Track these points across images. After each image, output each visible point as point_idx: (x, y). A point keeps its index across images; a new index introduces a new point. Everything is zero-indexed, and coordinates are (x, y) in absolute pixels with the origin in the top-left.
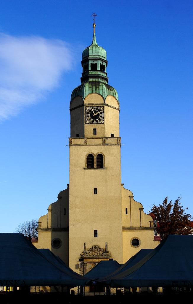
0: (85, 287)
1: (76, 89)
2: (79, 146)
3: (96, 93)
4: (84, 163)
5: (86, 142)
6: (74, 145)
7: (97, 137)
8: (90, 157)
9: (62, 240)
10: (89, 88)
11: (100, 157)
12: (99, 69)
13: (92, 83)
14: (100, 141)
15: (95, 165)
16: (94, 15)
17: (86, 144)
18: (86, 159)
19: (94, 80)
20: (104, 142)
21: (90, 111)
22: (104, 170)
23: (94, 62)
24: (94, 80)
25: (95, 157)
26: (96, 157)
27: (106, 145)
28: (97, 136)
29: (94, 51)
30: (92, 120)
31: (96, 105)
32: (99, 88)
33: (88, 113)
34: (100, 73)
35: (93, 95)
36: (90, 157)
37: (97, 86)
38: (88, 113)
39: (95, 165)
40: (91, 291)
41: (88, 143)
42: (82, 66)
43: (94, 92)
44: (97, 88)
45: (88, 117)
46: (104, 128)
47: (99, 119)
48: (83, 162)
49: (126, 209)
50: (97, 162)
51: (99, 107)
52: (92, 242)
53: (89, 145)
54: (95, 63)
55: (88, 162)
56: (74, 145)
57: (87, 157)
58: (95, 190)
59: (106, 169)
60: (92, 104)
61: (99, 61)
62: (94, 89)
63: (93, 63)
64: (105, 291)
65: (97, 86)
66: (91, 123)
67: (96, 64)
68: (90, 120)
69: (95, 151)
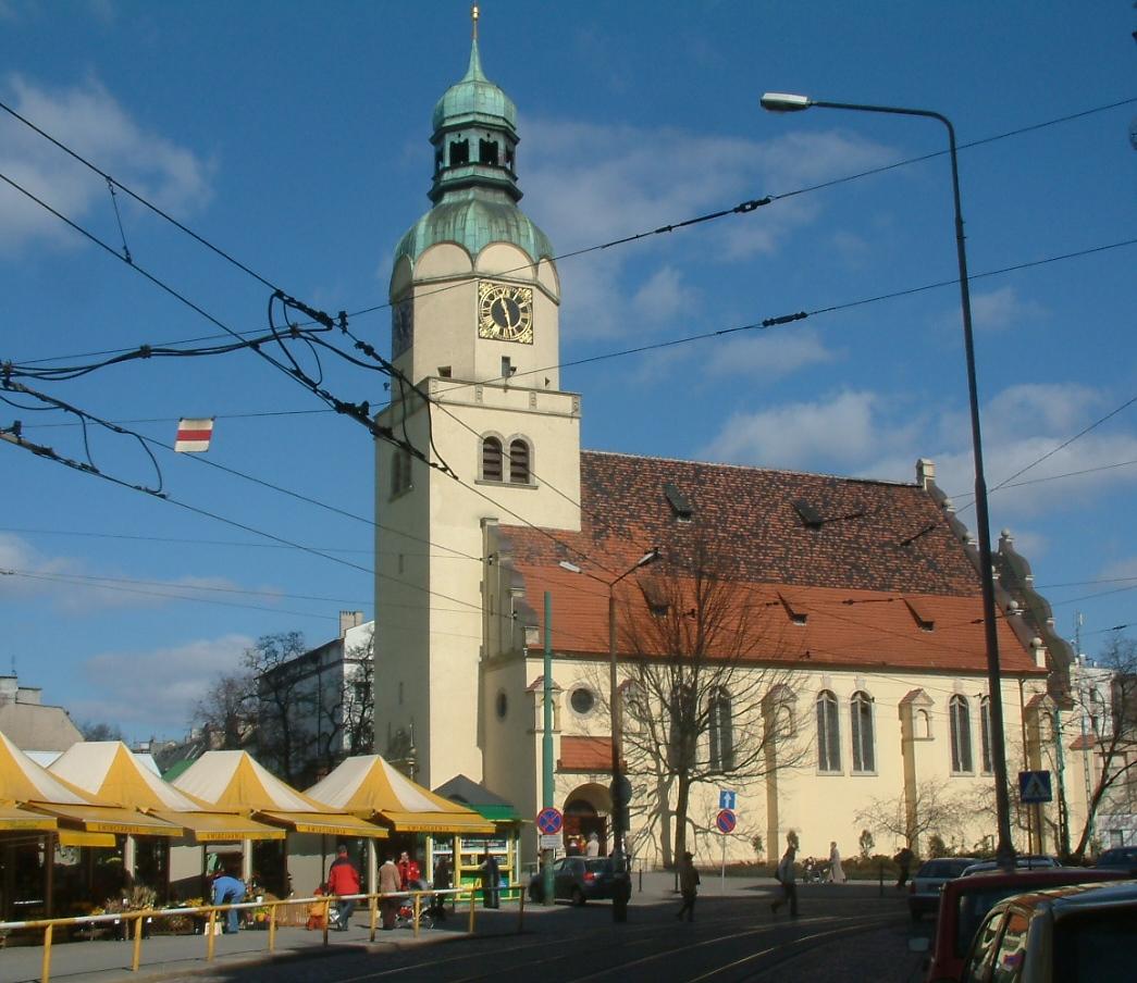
8: (492, 445)
11: (521, 447)
23: (488, 135)
25: (506, 449)
30: (496, 329)
32: (518, 228)
44: (514, 230)
45: (486, 315)
46: (583, 444)
51: (517, 288)
63: (486, 139)
66: (495, 338)
67: (496, 143)
68: (491, 327)
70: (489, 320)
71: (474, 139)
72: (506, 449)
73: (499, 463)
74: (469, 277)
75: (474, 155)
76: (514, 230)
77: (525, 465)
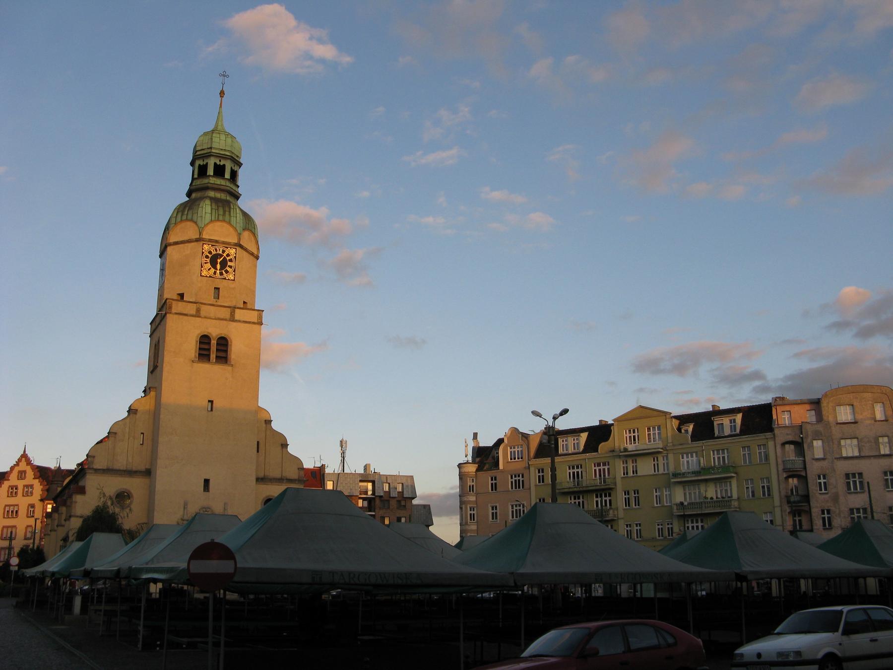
0: (644, 585)
1: (181, 205)
2: (185, 317)
3: (224, 221)
5: (198, 310)
6: (176, 314)
7: (219, 304)
8: (204, 340)
9: (135, 496)
11: (224, 343)
12: (227, 175)
13: (214, 200)
14: (226, 313)
15: (213, 356)
16: (224, 76)
17: (198, 315)
19: (218, 195)
20: (198, 310)
21: (210, 252)
22: (230, 368)
24: (218, 195)
25: (214, 342)
27: (236, 321)
28: (221, 302)
29: (222, 142)
30: (213, 270)
31: (224, 243)
33: (207, 257)
34: (213, 180)
35: (219, 224)
36: (223, 342)
37: (227, 209)
38: (207, 257)
39: (213, 356)
40: (656, 590)
41: (203, 313)
42: (192, 164)
43: (221, 218)
47: (227, 272)
48: (191, 347)
49: (258, 442)
52: (198, 501)
53: (205, 317)
55: (200, 349)
56: (176, 314)
59: (232, 366)
60: (217, 242)
61: (229, 161)
62: (221, 212)
63: (218, 163)
64: (207, 595)
65: (227, 209)
67: (224, 165)
69: (215, 330)
70: (209, 266)
71: (211, 162)
72: (214, 342)
74: (197, 240)
75: (210, 171)
77: (226, 351)
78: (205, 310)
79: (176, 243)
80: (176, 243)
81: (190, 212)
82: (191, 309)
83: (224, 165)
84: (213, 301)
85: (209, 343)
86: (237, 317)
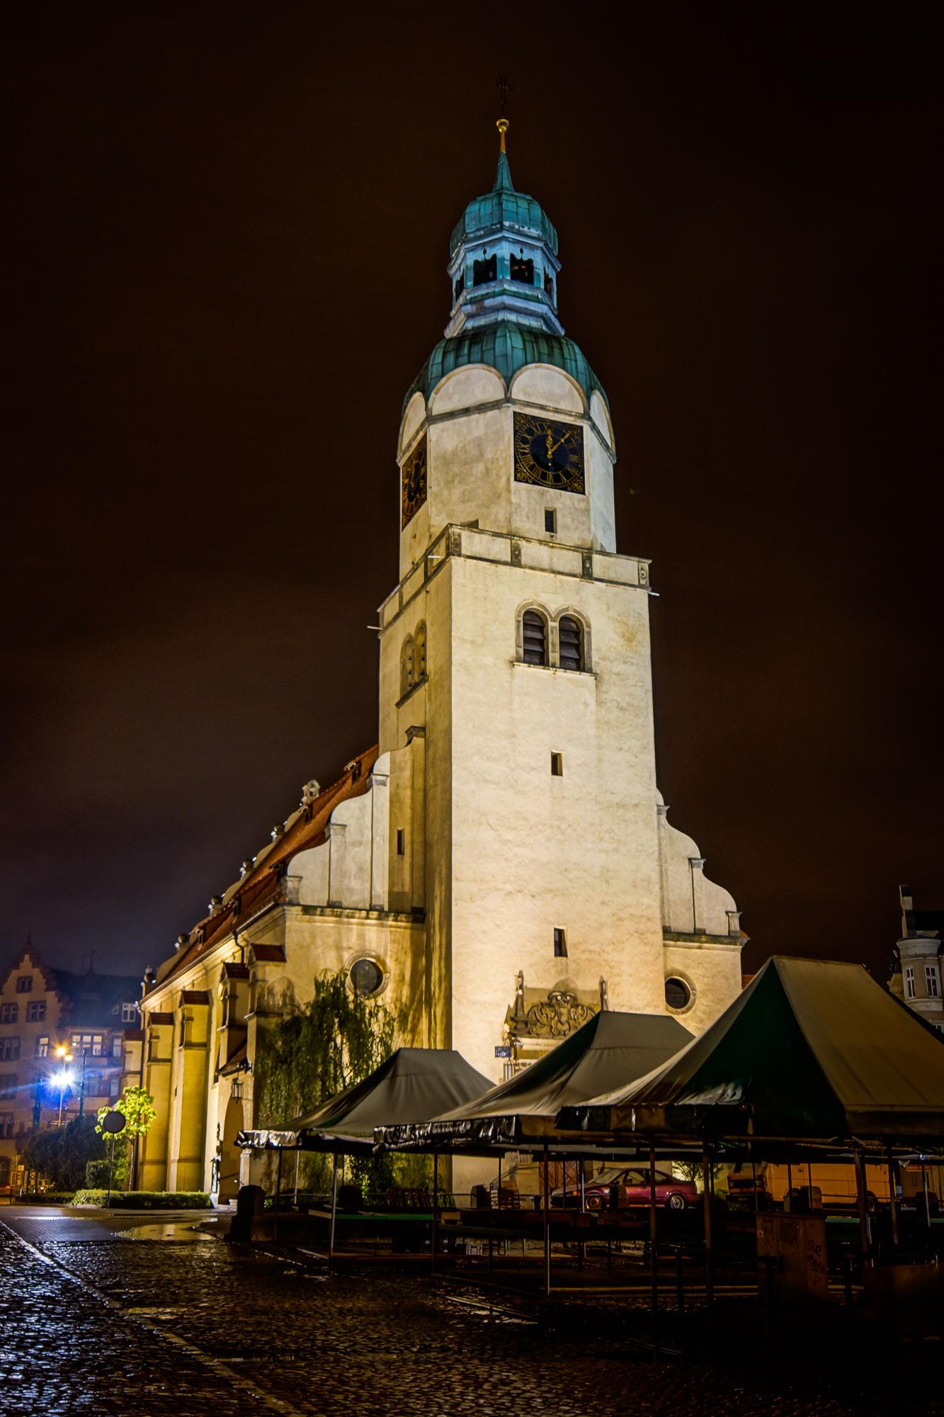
4: (512, 642)
8: (533, 621)
10: (524, 341)
17: (515, 560)
18: (518, 627)
25: (553, 625)
26: (556, 624)
32: (561, 349)
44: (556, 351)
48: (508, 638)
50: (563, 644)
54: (525, 259)
55: (526, 640)
57: (521, 619)
58: (556, 759)
63: (518, 256)
67: (530, 262)
68: (550, 521)
72: (553, 625)
73: (542, 642)
76: (556, 351)
77: (578, 647)
78: (531, 552)
79: (451, 415)
80: (451, 415)
81: (476, 349)
82: (501, 549)
83: (530, 262)
84: (544, 534)
85: (542, 628)
86: (597, 572)
